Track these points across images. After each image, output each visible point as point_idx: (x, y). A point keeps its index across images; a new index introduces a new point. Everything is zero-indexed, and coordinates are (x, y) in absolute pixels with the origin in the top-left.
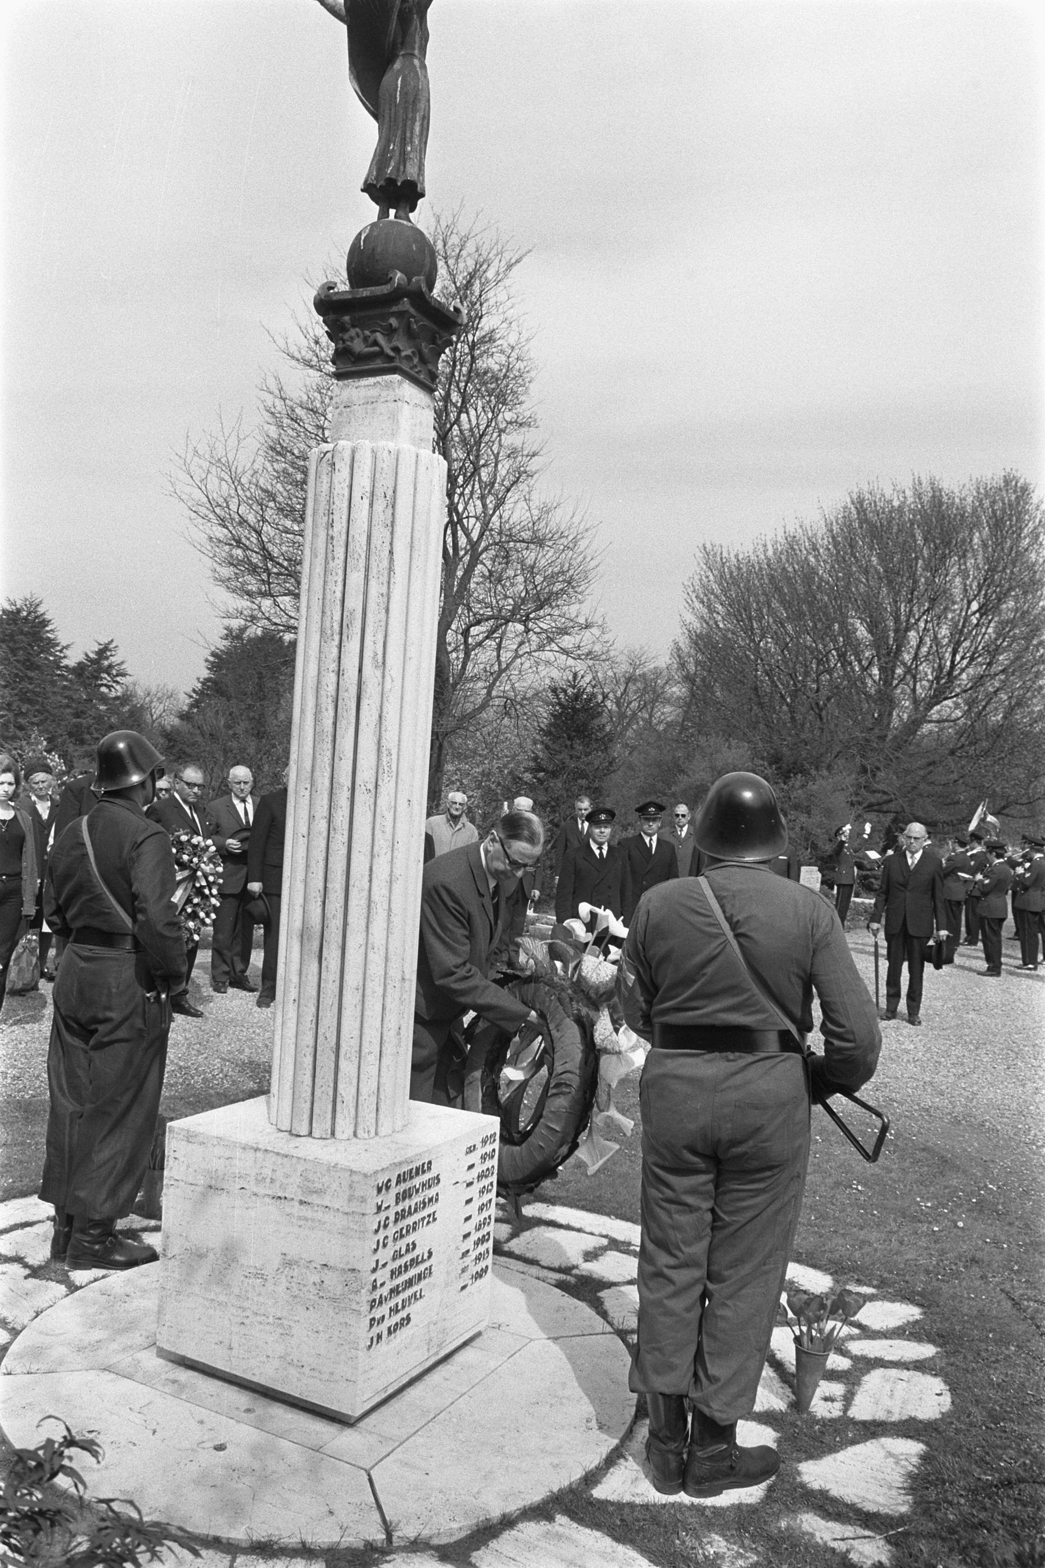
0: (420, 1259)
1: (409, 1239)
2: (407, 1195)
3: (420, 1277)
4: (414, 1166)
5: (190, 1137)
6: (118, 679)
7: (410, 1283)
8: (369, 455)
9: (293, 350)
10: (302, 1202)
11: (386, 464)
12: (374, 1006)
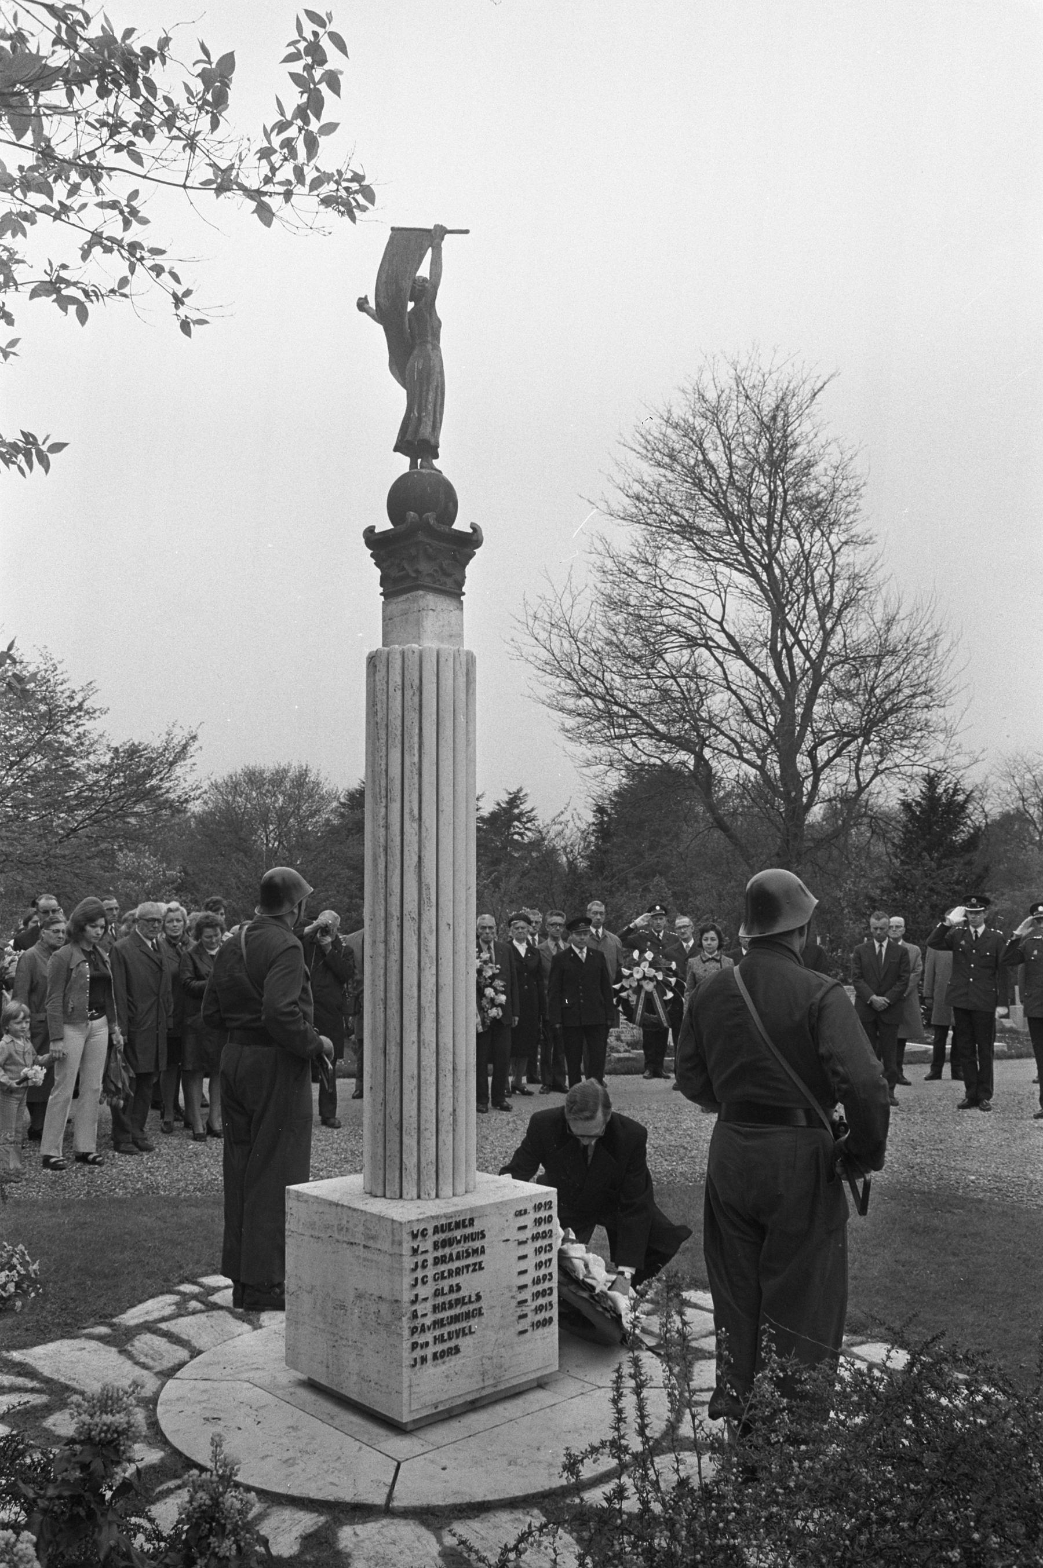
0: (467, 1300)
1: (454, 1281)
2: (448, 1243)
3: (468, 1316)
4: (453, 1220)
5: (299, 1195)
6: (529, 825)
7: (455, 1319)
8: (398, 657)
9: (616, 507)
10: (365, 1247)
11: (413, 662)
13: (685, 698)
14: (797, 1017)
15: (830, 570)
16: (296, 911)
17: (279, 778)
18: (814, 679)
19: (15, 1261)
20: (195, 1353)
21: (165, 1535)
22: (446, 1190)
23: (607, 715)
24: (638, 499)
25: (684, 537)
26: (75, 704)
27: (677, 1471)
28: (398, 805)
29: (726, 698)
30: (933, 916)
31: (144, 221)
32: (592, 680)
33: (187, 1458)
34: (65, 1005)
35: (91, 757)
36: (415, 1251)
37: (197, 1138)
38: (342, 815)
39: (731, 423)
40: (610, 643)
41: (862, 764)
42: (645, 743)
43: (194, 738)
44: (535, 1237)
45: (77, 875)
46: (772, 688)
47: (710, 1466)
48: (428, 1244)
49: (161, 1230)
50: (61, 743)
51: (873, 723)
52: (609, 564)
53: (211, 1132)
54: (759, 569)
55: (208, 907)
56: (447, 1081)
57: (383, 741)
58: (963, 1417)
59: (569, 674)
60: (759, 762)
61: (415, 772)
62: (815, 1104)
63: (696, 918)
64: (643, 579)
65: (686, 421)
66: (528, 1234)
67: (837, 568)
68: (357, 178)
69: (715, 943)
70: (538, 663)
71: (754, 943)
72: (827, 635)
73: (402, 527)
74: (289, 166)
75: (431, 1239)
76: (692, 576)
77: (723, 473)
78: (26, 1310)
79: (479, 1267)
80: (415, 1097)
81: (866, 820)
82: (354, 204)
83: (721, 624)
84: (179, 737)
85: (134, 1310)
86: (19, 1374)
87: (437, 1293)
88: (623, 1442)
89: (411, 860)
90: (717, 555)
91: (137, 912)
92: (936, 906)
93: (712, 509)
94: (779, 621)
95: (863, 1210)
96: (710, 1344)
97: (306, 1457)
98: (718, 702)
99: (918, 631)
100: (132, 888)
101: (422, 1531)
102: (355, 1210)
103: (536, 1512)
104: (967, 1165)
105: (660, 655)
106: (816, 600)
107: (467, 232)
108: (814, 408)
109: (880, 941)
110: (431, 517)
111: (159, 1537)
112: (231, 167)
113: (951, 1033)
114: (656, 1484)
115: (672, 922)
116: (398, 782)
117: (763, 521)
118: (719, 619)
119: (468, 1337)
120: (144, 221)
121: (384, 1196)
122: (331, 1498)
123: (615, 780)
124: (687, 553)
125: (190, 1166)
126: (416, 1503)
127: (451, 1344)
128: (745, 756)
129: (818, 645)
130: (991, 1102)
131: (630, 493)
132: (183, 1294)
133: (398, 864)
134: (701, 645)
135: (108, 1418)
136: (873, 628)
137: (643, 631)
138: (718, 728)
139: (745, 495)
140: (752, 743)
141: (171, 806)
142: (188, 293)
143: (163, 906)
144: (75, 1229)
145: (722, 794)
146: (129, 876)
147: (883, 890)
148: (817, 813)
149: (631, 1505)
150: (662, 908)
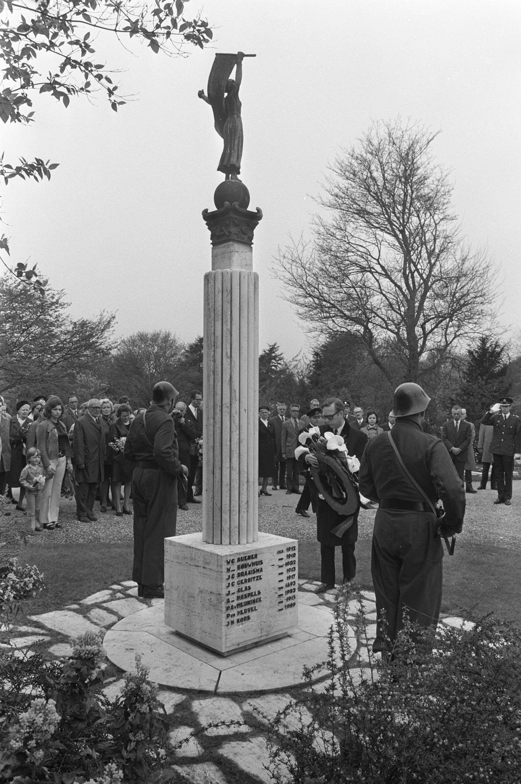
1: (247, 585)
2: (243, 566)
3: (254, 602)
4: (247, 555)
5: (171, 542)
6: (279, 362)
7: (248, 603)
9: (325, 200)
10: (204, 568)
11: (227, 278)
12: (235, 492)
13: (359, 298)
14: (420, 457)
15: (434, 233)
16: (170, 403)
17: (155, 338)
18: (425, 289)
19: (32, 573)
20: (120, 618)
21: (111, 702)
22: (243, 540)
23: (320, 307)
24: (337, 196)
25: (360, 216)
26: (54, 300)
27: (361, 676)
28: (220, 350)
29: (380, 298)
30: (483, 408)
31: (92, 51)
32: (313, 288)
33: (118, 667)
34: (47, 450)
35: (63, 327)
36: (228, 570)
37: (118, 514)
38: (187, 356)
39: (385, 157)
40: (322, 270)
41: (448, 331)
42: (339, 320)
43: (114, 317)
44: (287, 564)
45: (56, 386)
46: (403, 293)
47: (377, 675)
48: (234, 567)
49: (102, 559)
50: (48, 320)
51: (454, 311)
52: (322, 230)
53: (125, 512)
54: (398, 232)
55: (121, 402)
56: (244, 487)
57: (212, 318)
58: (501, 653)
59: (301, 285)
60: (396, 330)
61: (229, 333)
62: (428, 500)
63: (364, 408)
64: (339, 237)
65: (362, 156)
66: (283, 562)
67: (438, 232)
68: (204, 24)
69: (375, 420)
70: (285, 280)
71: (398, 420)
72: (432, 266)
73: (222, 209)
74: (169, 18)
75: (236, 564)
76: (363, 236)
77: (380, 183)
78: (38, 596)
79: (259, 578)
80: (228, 495)
81: (450, 360)
82: (202, 38)
83: (378, 260)
84: (107, 317)
85: (90, 597)
86: (36, 627)
87: (239, 590)
88: (334, 663)
89: (226, 378)
90: (377, 225)
91: (88, 403)
92: (485, 403)
93: (375, 201)
94: (408, 259)
95: (451, 552)
96: (374, 616)
97: (175, 668)
98: (376, 300)
99: (478, 264)
100: (84, 392)
101: (232, 703)
102: (199, 550)
103: (288, 695)
104: (499, 531)
105: (347, 276)
106: (427, 248)
107: (255, 55)
108: (429, 149)
109: (457, 420)
110: (236, 204)
111: (108, 704)
112: (137, 21)
113: (491, 466)
114: (351, 684)
115: (352, 410)
116: (220, 338)
117: (400, 208)
118: (377, 258)
119: (254, 612)
120: (92, 51)
121: (213, 543)
122: (188, 687)
123: (323, 339)
124: (361, 224)
125: (116, 528)
126: (230, 691)
127: (246, 615)
128: (390, 327)
129: (427, 272)
130: (511, 500)
131: (333, 193)
132: (113, 590)
133: (220, 379)
134: (367, 271)
135: (89, 648)
136: (455, 263)
137: (338, 264)
138: (375, 313)
139: (391, 194)
140: (393, 321)
141: (103, 351)
142: (115, 88)
143: (102, 401)
144: (60, 558)
145: (376, 346)
146: (83, 386)
147: (457, 395)
148: (424, 357)
149: (338, 693)
150: (348, 403)
